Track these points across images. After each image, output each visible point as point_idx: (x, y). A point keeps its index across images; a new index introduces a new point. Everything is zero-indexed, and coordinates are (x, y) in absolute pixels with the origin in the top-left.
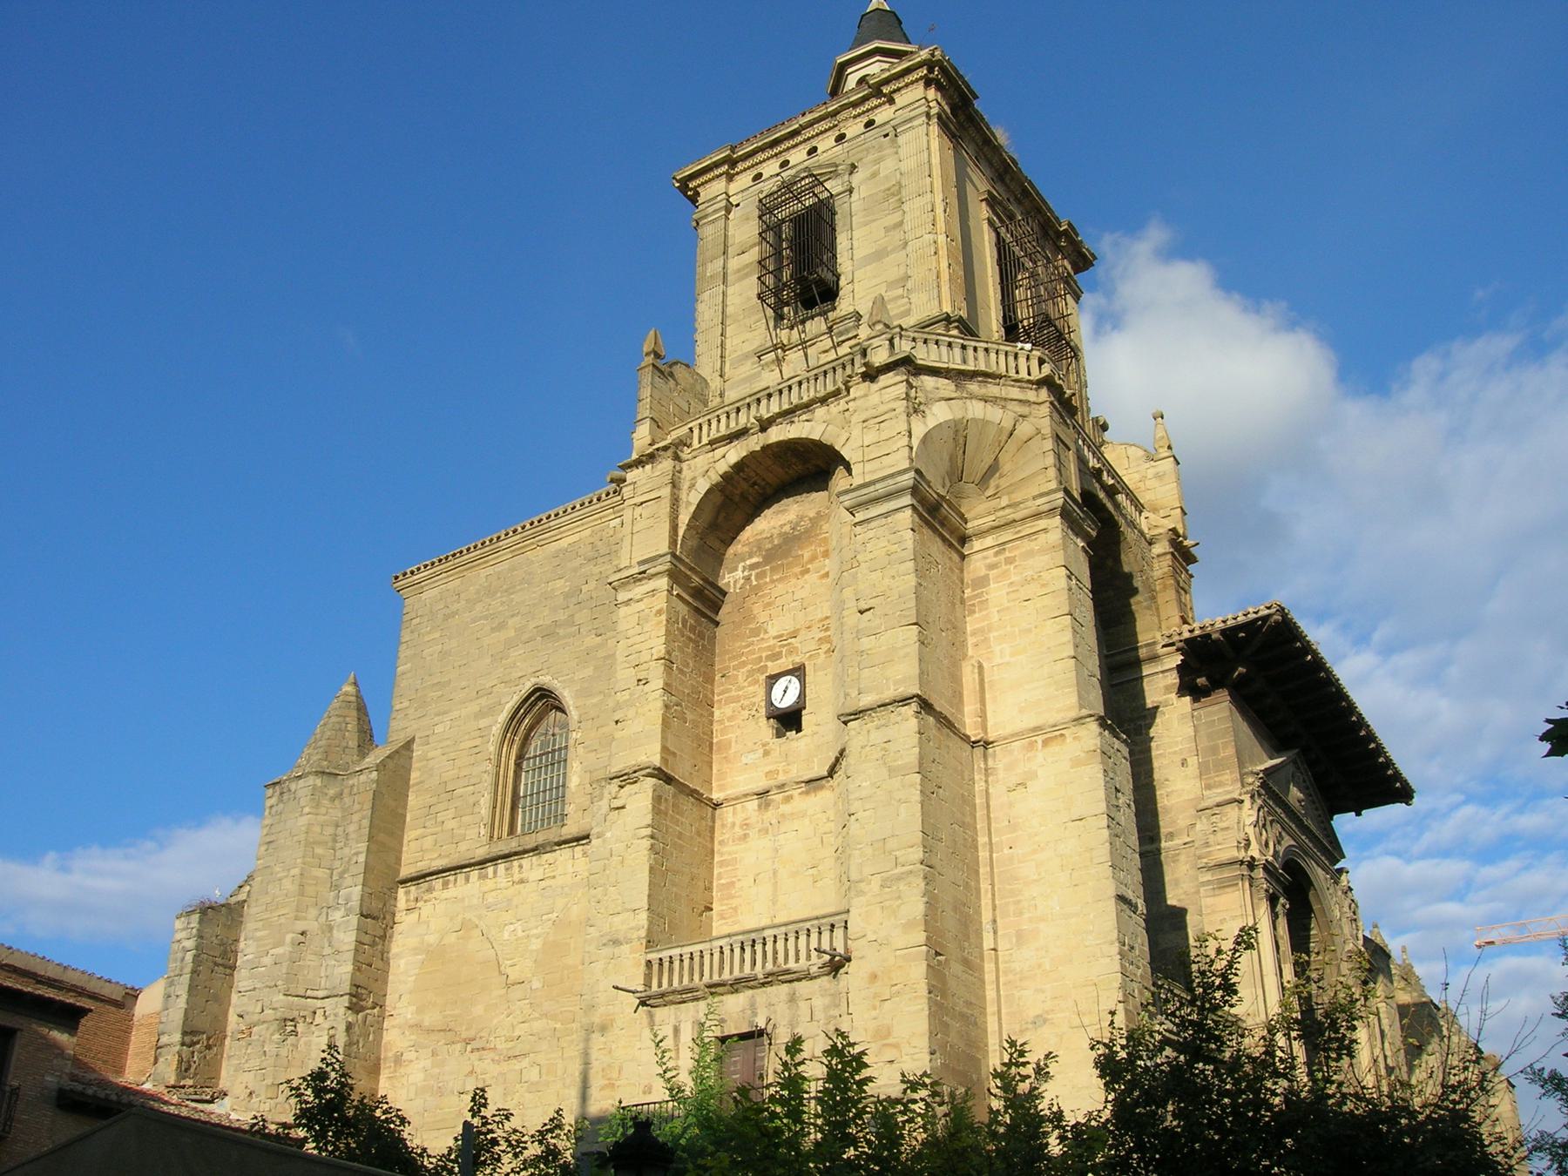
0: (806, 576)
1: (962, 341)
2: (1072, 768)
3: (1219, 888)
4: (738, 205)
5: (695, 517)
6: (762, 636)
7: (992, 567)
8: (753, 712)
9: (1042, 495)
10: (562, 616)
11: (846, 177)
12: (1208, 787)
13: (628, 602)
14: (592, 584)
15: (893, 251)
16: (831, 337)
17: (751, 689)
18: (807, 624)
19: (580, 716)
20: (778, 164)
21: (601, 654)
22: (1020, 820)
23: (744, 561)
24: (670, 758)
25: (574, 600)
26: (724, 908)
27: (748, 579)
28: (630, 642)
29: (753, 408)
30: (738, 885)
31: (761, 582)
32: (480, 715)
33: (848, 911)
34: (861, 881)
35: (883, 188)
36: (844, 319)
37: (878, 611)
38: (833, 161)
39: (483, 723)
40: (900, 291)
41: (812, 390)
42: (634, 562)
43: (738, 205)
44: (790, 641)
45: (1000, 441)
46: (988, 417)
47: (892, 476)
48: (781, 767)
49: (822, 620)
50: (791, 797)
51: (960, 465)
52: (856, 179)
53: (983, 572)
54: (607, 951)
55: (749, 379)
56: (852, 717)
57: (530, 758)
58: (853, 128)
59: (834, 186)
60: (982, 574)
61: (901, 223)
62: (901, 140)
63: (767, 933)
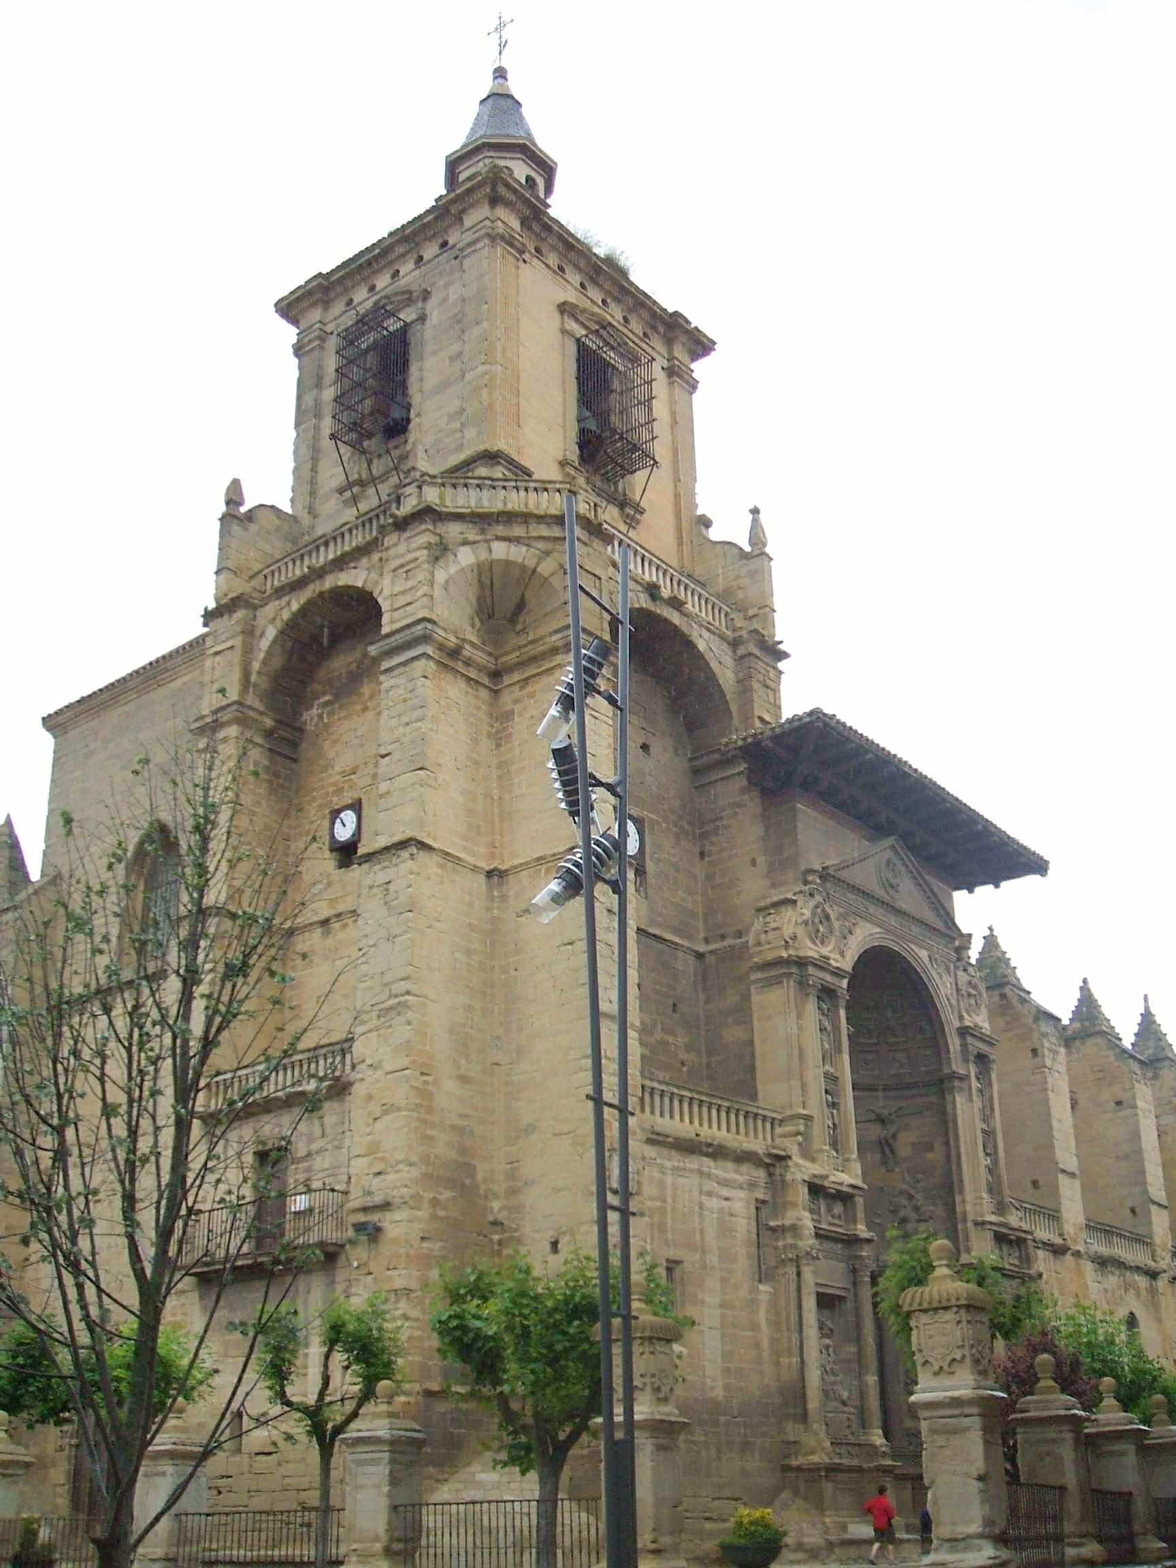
5: (264, 662)
7: (516, 701)
11: (420, 304)
12: (774, 885)
23: (318, 698)
27: (321, 716)
29: (306, 558)
37: (395, 756)
47: (408, 626)
51: (489, 604)
52: (433, 302)
53: (509, 707)
58: (430, 251)
59: (408, 315)
62: (467, 262)
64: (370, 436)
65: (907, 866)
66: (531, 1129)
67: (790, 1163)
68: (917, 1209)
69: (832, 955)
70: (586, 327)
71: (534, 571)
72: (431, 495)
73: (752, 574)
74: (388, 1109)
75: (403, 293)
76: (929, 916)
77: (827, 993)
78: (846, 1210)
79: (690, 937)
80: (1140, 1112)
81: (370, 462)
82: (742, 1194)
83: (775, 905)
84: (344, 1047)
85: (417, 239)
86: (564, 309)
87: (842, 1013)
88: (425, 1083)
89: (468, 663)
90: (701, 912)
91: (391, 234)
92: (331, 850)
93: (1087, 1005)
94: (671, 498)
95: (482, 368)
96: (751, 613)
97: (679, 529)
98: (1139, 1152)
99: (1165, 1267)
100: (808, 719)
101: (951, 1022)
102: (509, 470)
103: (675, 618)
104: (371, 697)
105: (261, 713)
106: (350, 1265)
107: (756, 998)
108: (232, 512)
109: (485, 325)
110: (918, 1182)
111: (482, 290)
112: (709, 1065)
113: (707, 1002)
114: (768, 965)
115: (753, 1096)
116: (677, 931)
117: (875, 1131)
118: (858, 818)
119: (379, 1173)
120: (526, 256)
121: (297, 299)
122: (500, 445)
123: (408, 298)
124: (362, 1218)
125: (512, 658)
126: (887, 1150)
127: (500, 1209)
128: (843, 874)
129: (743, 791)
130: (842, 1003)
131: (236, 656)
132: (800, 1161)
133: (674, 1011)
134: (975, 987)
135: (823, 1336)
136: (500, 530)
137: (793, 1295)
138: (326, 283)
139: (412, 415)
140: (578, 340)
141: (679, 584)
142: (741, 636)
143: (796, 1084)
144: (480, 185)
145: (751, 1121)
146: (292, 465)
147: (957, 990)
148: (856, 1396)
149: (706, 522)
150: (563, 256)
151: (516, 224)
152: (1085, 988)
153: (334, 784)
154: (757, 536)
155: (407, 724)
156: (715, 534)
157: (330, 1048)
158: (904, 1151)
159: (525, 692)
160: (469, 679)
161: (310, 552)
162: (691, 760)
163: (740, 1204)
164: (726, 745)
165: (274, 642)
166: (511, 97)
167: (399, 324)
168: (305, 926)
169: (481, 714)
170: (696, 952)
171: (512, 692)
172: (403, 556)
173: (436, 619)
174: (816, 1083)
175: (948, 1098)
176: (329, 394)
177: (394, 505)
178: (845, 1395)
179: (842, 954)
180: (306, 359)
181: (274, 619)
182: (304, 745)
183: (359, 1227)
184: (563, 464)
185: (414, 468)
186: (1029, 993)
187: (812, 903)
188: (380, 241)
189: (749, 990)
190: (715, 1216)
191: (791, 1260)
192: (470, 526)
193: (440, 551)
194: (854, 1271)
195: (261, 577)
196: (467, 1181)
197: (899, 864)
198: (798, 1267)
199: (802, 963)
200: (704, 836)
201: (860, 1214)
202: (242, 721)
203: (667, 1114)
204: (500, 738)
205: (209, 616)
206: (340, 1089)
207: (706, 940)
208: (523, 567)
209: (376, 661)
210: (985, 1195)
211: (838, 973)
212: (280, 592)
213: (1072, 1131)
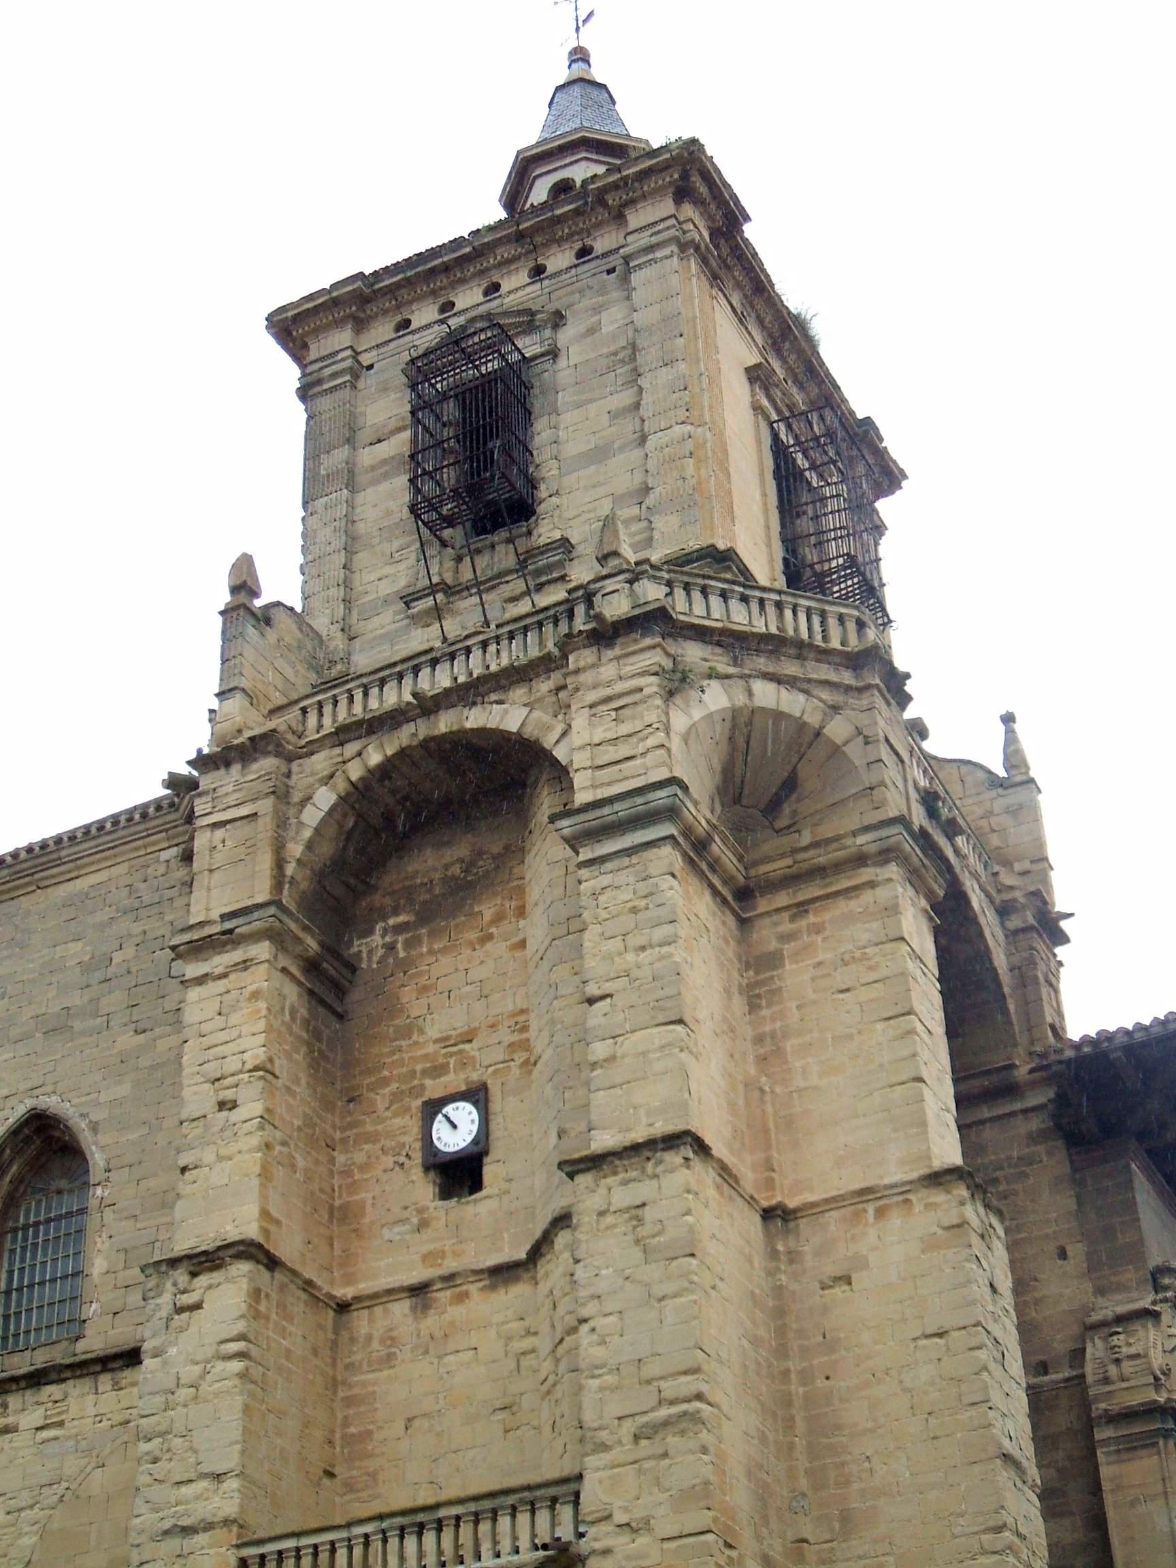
0: (489, 946)
1: (741, 589)
2: (923, 1252)
4: (370, 367)
5: (310, 846)
6: (415, 1037)
7: (786, 938)
8: (402, 1159)
9: (867, 829)
10: (77, 999)
11: (548, 333)
12: (1101, 1291)
13: (201, 980)
14: (130, 951)
15: (621, 449)
17: (398, 1121)
18: (491, 1020)
19: (108, 1161)
21: (144, 1062)
22: (842, 1335)
23: (384, 918)
24: (273, 1228)
25: (99, 975)
27: (391, 948)
28: (206, 1042)
30: (378, 1436)
31: (413, 953)
33: (580, 1477)
34: (600, 1428)
35: (605, 351)
36: (549, 547)
38: (525, 306)
40: (635, 510)
41: (504, 654)
42: (215, 915)
43: (370, 367)
44: (461, 1047)
45: (800, 745)
46: (785, 708)
47: (640, 791)
48: (448, 1245)
49: (514, 1015)
50: (466, 1295)
52: (564, 336)
53: (774, 945)
54: (174, 1544)
55: (390, 638)
56: (582, 1166)
58: (559, 259)
59: (529, 345)
61: (637, 406)
63: (442, 1513)
71: (818, 734)
73: (1015, 812)
75: (519, 313)
83: (1120, 1319)
85: (538, 239)
92: (427, 1168)
95: (679, 430)
121: (316, 310)
123: (529, 320)
125: (778, 867)
131: (265, 826)
138: (367, 291)
142: (1015, 900)
144: (666, 167)
159: (803, 923)
168: (375, 1296)
169: (730, 954)
171: (776, 924)
172: (609, 684)
180: (325, 403)
181: (331, 776)
182: (355, 995)
192: (718, 650)
195: (295, 712)
208: (802, 726)
212: (343, 734)
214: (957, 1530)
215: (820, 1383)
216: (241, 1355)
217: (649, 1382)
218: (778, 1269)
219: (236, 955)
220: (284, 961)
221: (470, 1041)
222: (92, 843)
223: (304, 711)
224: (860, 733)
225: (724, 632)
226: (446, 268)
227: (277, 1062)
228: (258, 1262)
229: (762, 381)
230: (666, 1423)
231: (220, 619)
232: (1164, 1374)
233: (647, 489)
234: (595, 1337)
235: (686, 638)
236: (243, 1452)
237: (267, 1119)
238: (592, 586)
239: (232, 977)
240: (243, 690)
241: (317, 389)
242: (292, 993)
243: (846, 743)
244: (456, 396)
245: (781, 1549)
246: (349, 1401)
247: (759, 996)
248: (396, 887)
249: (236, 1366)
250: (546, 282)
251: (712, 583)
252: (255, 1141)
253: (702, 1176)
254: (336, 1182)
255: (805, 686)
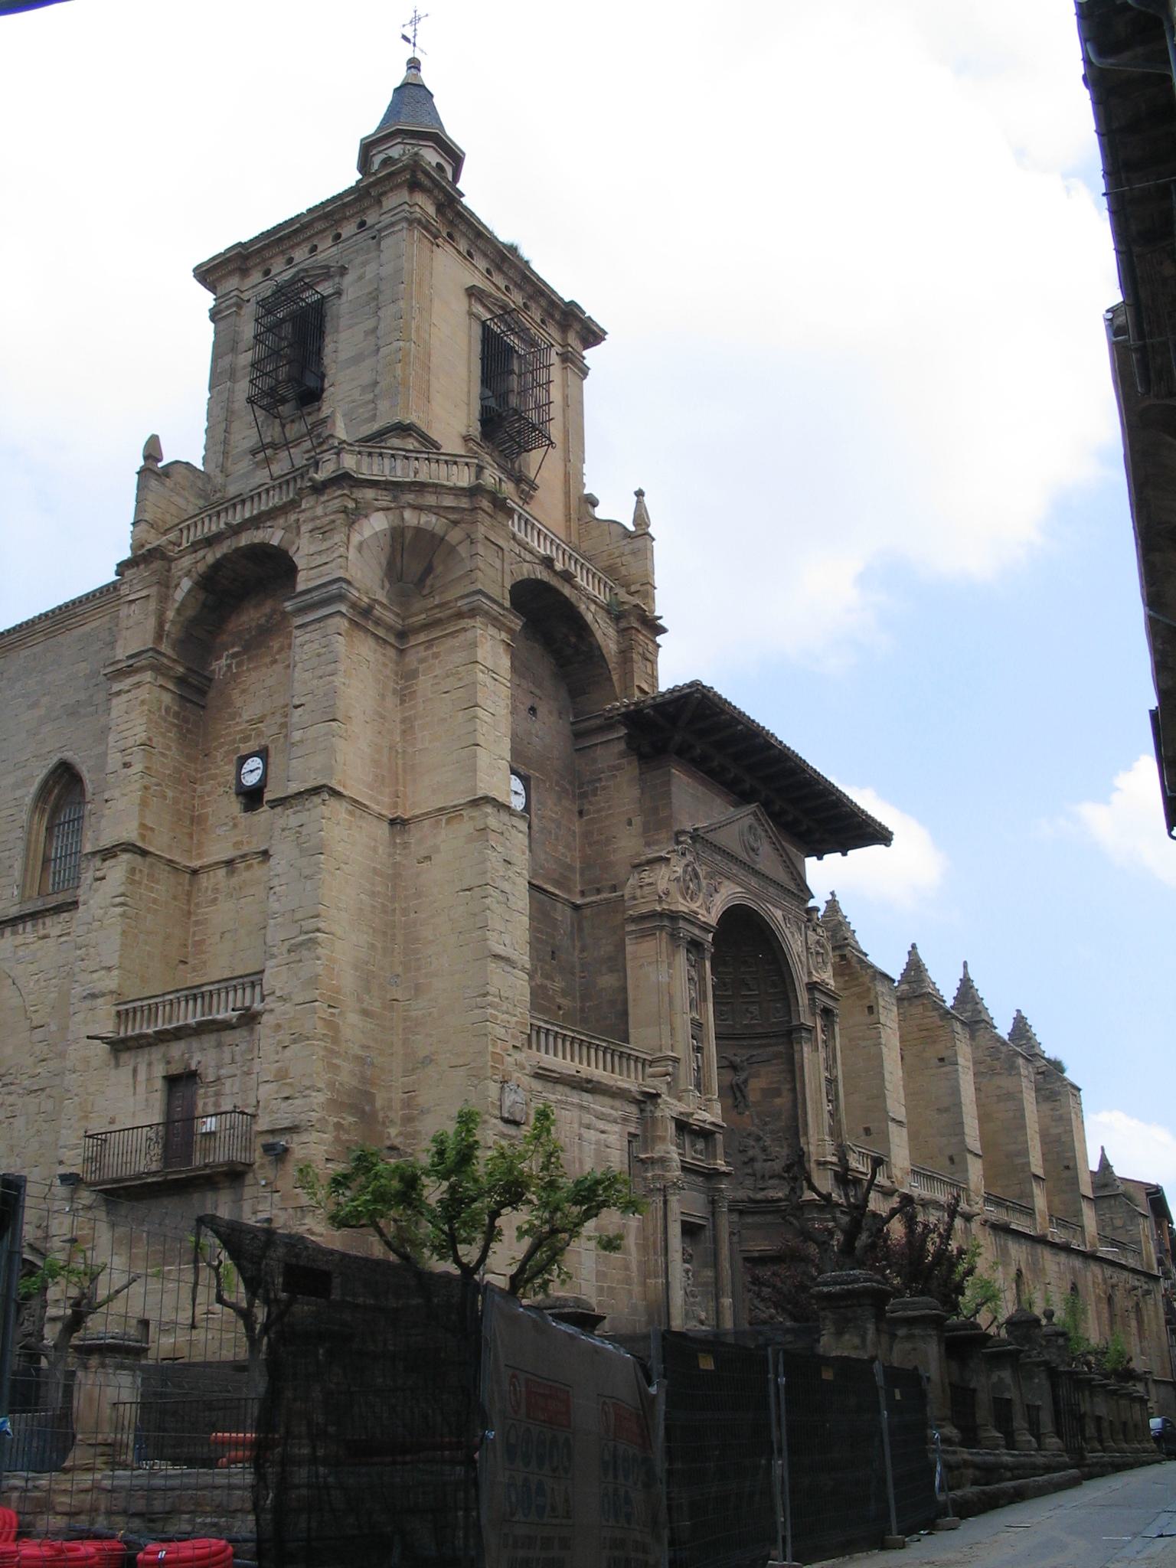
0: (274, 666)
3: (641, 937)
5: (179, 611)
6: (237, 720)
7: (422, 661)
9: (462, 597)
11: (337, 279)
12: (648, 844)
13: (118, 693)
16: (311, 439)
19: (94, 788)
20: (284, 261)
23: (227, 650)
25: (94, 681)
26: (196, 962)
27: (229, 666)
29: (223, 515)
32: (16, 786)
33: (262, 972)
39: (18, 793)
52: (349, 279)
54: (88, 1003)
57: (60, 824)
58: (348, 229)
59: (325, 289)
60: (413, 667)
63: (205, 989)
64: (283, 401)
65: (766, 831)
66: (428, 1060)
67: (659, 1101)
68: (764, 1149)
69: (700, 911)
70: (490, 311)
71: (442, 539)
72: (349, 462)
74: (298, 1038)
76: (782, 876)
77: (695, 945)
78: (706, 1148)
79: (569, 891)
80: (960, 1069)
81: (283, 426)
82: (616, 1128)
83: (650, 862)
84: (253, 980)
86: (473, 293)
87: (708, 964)
88: (333, 1014)
89: (378, 622)
90: (578, 866)
91: (310, 211)
92: (238, 794)
93: (915, 967)
94: (561, 477)
96: (633, 588)
97: (567, 506)
98: (959, 1105)
99: (978, 1211)
100: (688, 690)
101: (801, 978)
102: (420, 442)
103: (567, 591)
104: (279, 652)
105: (174, 661)
106: (257, 1184)
107: (629, 948)
108: (150, 467)
109: (402, 304)
110: (766, 1124)
111: (399, 271)
112: (582, 1010)
113: (582, 950)
114: (643, 918)
115: (626, 1040)
116: (557, 884)
117: (730, 1077)
118: (723, 783)
119: (287, 1098)
120: (440, 241)
122: (412, 418)
123: (327, 273)
124: (270, 1139)
126: (738, 1094)
127: (397, 1136)
128: (710, 836)
129: (622, 755)
130: (708, 955)
131: (152, 605)
132: (668, 1099)
133: (553, 958)
134: (823, 947)
135: (685, 1261)
136: (410, 498)
137: (660, 1222)
139: (326, 385)
140: (484, 323)
141: (570, 559)
143: (666, 1029)
145: (624, 1060)
146: (205, 424)
147: (808, 949)
148: (712, 1315)
149: (593, 502)
150: (472, 243)
151: (431, 210)
152: (913, 951)
153: (241, 731)
154: (641, 517)
155: (321, 677)
156: (600, 513)
157: (241, 980)
158: (753, 1097)
160: (377, 637)
161: (226, 510)
162: (573, 724)
163: (615, 1137)
164: (610, 710)
165: (190, 591)
166: (423, 87)
167: (316, 297)
169: (388, 672)
170: (573, 903)
173: (348, 577)
174: (683, 1030)
175: (796, 1047)
176: (246, 358)
177: (312, 470)
178: (703, 1315)
179: (708, 910)
180: (223, 324)
182: (212, 694)
183: (268, 1149)
184: (467, 439)
185: (332, 436)
186: (866, 955)
187: (684, 862)
188: (298, 216)
189: (624, 940)
190: (593, 1147)
191: (659, 1189)
193: (354, 516)
194: (713, 1202)
196: (367, 1108)
197: (760, 831)
198: (665, 1196)
199: (673, 917)
200: (583, 796)
201: (720, 1150)
202: (156, 669)
203: (551, 1051)
204: (405, 695)
205: (122, 567)
206: (249, 1018)
207: (583, 894)
208: (433, 535)
209: (285, 615)
210: (827, 1138)
211: (705, 928)
213: (901, 1083)
214: (466, 995)
215: (413, 915)
216: (122, 904)
217: (296, 922)
218: (395, 853)
219: (136, 679)
220: (161, 681)
221: (262, 722)
222: (98, 601)
223: (181, 530)
224: (469, 537)
225: (387, 482)
226: (288, 236)
227: (155, 739)
228: (135, 853)
229: (476, 296)
230: (302, 944)
231: (137, 476)
232: (664, 894)
233: (376, 383)
234: (275, 897)
235: (364, 487)
236: (121, 956)
237: (147, 771)
238: (318, 457)
239: (133, 692)
240: (146, 521)
241: (219, 316)
242: (167, 698)
243: (457, 545)
244: (290, 320)
245: (380, 1005)
246: (197, 923)
247: (405, 695)
248: (235, 630)
249: (119, 910)
250: (340, 245)
251: (385, 451)
252: (138, 786)
253: (338, 810)
254: (196, 802)
255: (436, 510)
